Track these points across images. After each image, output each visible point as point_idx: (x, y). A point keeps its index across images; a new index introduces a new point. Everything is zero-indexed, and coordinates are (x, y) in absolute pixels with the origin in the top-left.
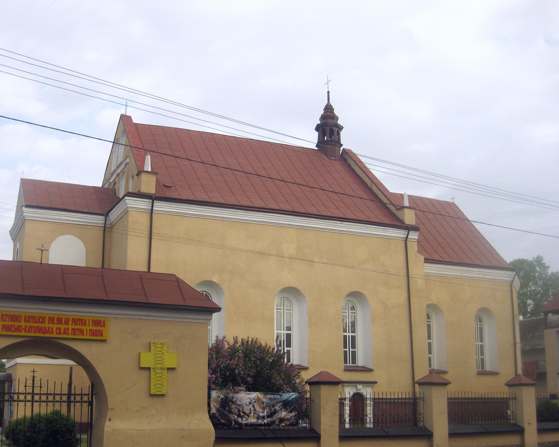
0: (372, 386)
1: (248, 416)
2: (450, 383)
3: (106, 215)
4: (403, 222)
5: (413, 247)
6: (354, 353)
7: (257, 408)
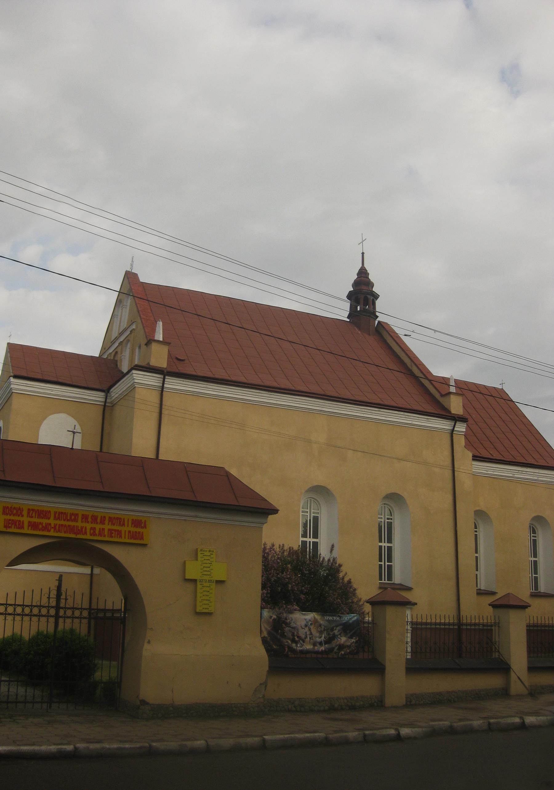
0: (411, 608)
1: (304, 641)
2: (530, 606)
3: (107, 391)
4: (449, 412)
5: (460, 442)
6: (390, 568)
7: (314, 632)
